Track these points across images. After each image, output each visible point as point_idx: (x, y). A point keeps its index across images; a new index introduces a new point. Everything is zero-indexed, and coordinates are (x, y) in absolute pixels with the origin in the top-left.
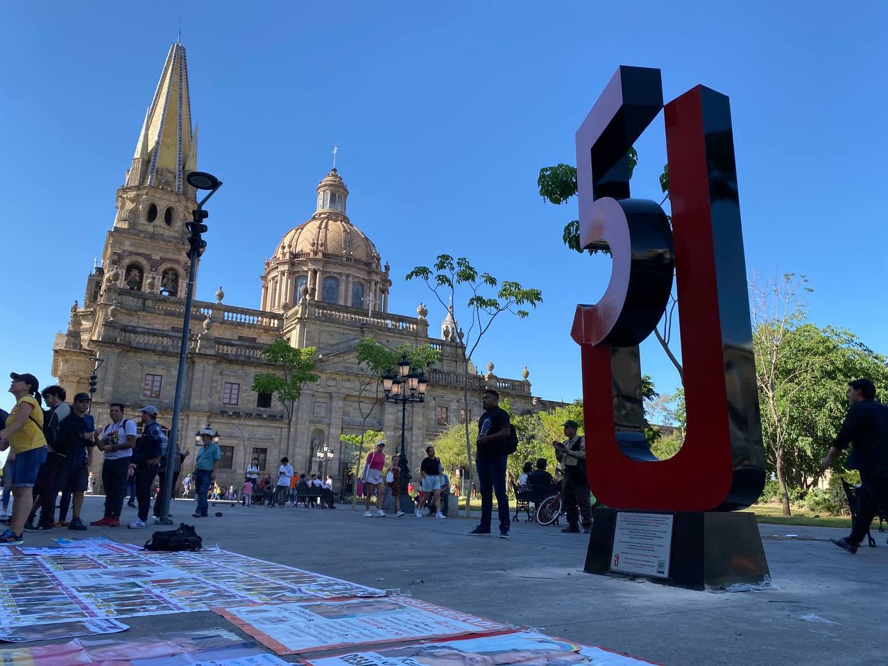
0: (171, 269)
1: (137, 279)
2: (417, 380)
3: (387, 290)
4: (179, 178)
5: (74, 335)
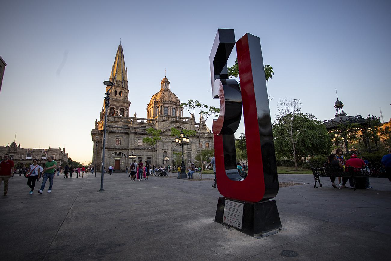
0: (121, 108)
1: (113, 112)
2: (186, 138)
3: (182, 110)
5: (97, 128)
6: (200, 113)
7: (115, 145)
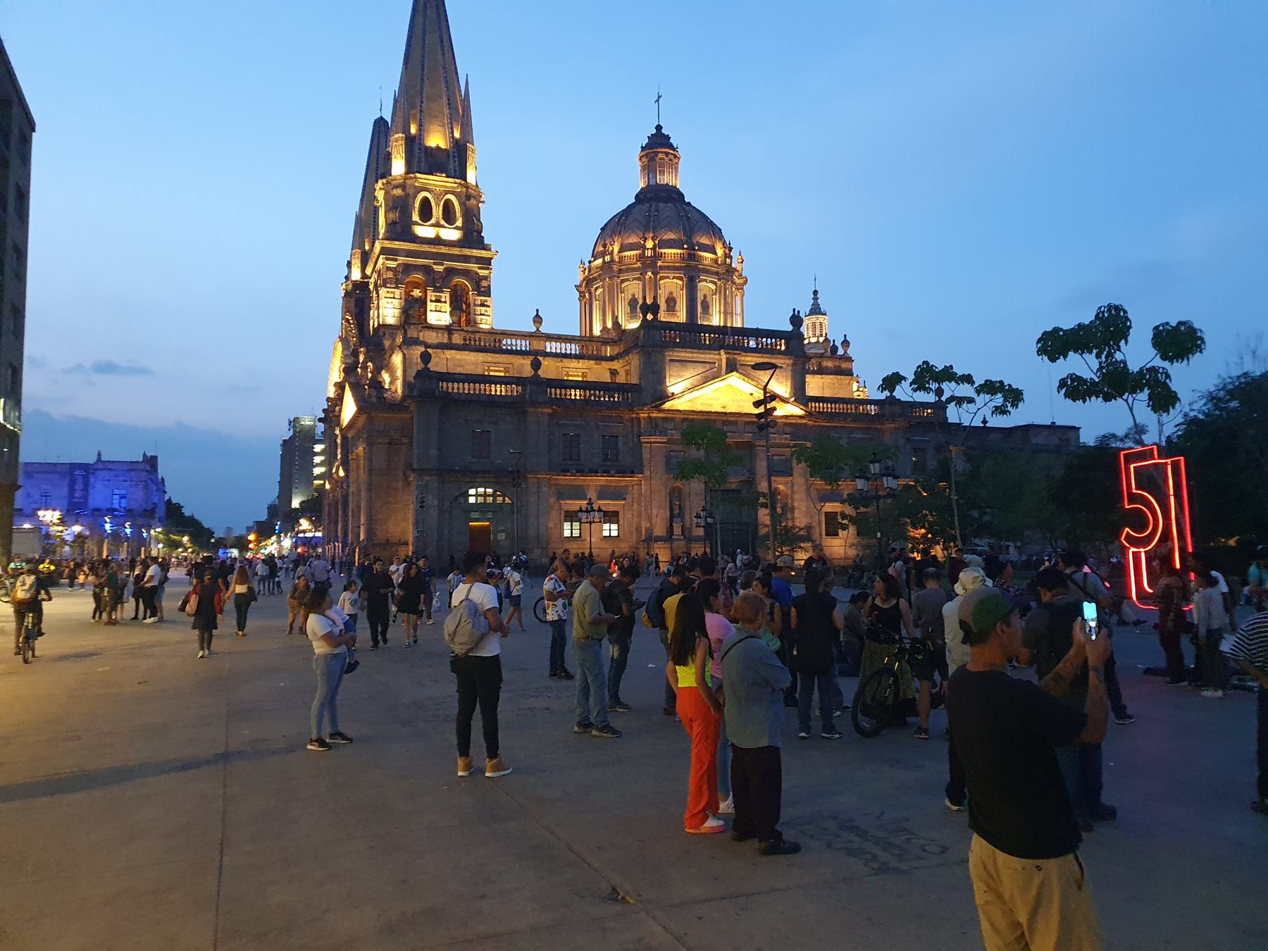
4: (454, 157)
7: (470, 459)
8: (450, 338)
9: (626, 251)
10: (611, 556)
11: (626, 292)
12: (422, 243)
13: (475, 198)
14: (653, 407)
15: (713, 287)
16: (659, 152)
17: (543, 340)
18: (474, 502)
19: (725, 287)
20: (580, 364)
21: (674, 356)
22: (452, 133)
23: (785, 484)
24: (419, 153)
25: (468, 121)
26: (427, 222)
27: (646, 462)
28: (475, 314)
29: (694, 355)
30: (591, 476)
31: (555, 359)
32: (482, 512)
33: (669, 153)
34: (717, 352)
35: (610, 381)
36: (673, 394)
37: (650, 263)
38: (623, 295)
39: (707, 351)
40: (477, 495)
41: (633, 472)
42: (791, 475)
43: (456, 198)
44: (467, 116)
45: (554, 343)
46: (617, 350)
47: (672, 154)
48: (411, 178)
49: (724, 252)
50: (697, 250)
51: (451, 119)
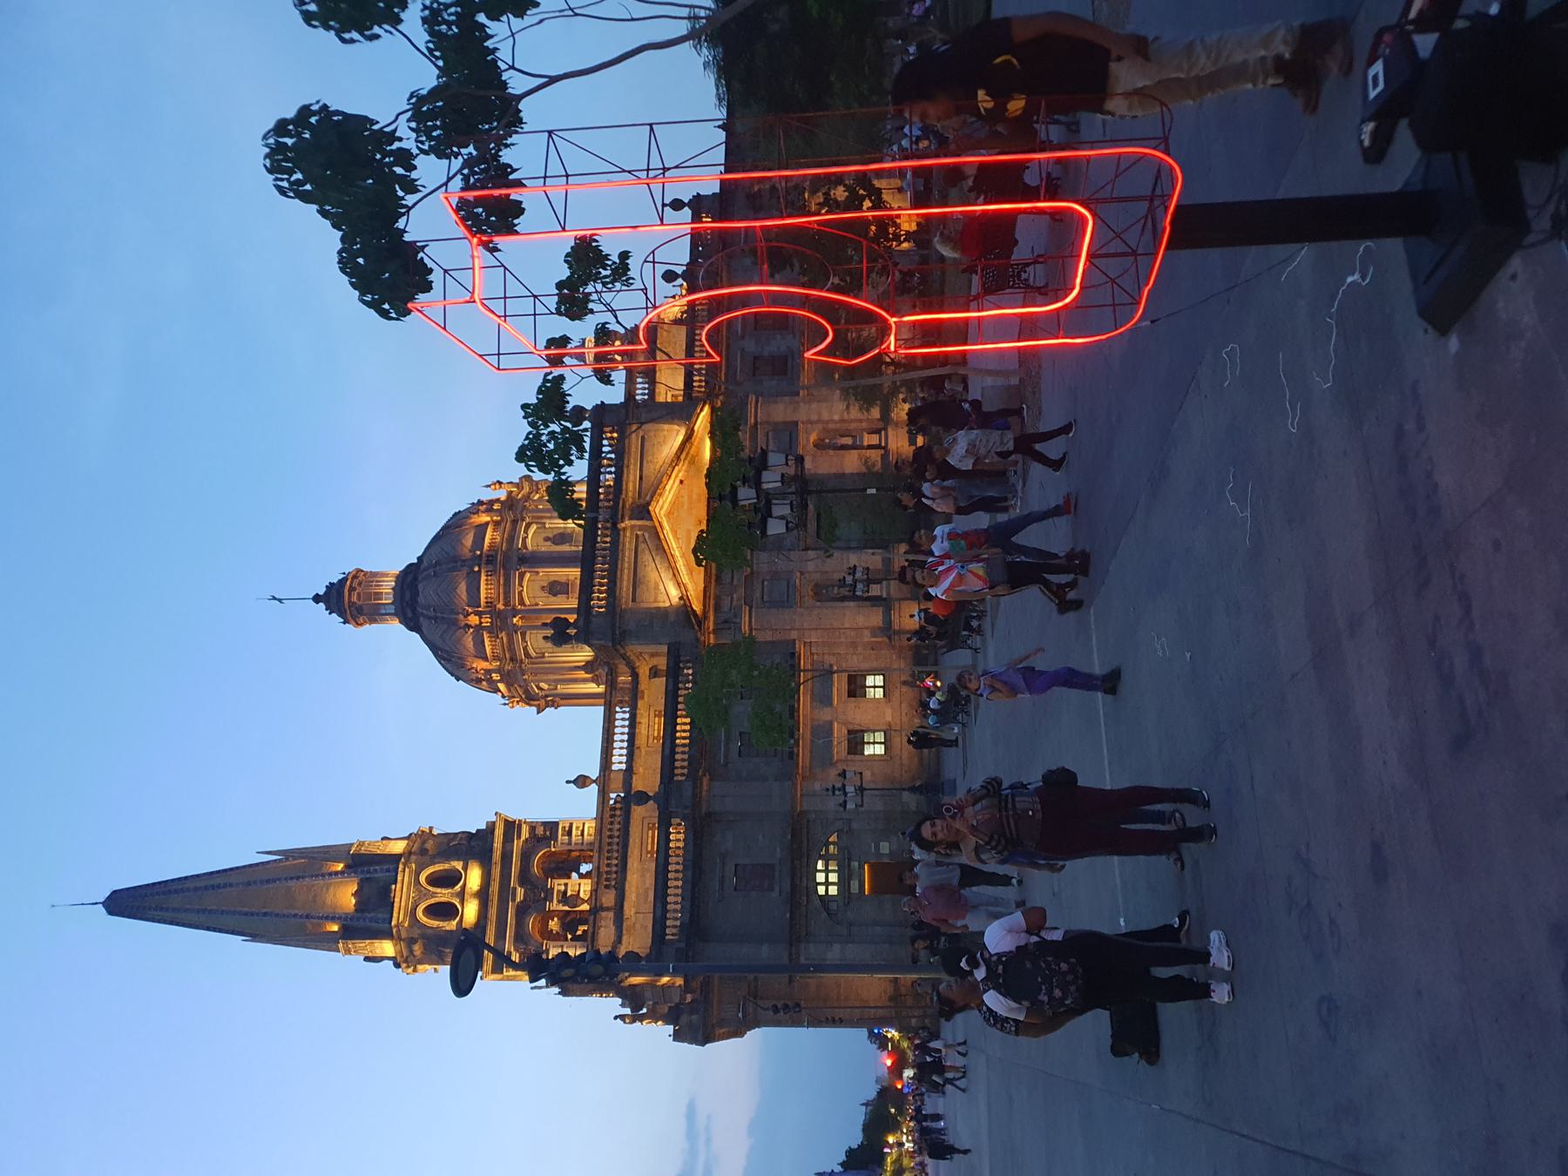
4: (369, 872)
6: (855, 566)
7: (775, 894)
8: (608, 909)
9: (485, 650)
10: (912, 687)
11: (543, 651)
12: (486, 917)
13: (424, 842)
14: (700, 626)
15: (534, 527)
16: (350, 601)
17: (609, 774)
18: (836, 887)
19: (533, 511)
20: (642, 721)
21: (628, 594)
22: (337, 873)
23: (808, 434)
24: (364, 920)
25: (318, 852)
26: (458, 910)
27: (777, 637)
28: (582, 844)
29: (626, 565)
30: (799, 716)
31: (635, 757)
32: (850, 878)
33: (351, 586)
34: (621, 533)
35: (665, 678)
36: (681, 598)
37: (500, 620)
38: (546, 655)
39: (620, 547)
40: (827, 883)
41: (793, 654)
42: (797, 422)
43: (424, 868)
44: (314, 853)
45: (613, 758)
46: (622, 667)
47: (352, 583)
48: (398, 931)
49: (483, 512)
50: (482, 552)
51: (317, 876)
